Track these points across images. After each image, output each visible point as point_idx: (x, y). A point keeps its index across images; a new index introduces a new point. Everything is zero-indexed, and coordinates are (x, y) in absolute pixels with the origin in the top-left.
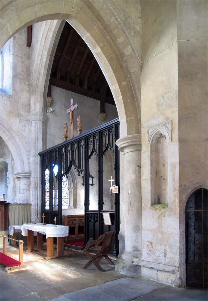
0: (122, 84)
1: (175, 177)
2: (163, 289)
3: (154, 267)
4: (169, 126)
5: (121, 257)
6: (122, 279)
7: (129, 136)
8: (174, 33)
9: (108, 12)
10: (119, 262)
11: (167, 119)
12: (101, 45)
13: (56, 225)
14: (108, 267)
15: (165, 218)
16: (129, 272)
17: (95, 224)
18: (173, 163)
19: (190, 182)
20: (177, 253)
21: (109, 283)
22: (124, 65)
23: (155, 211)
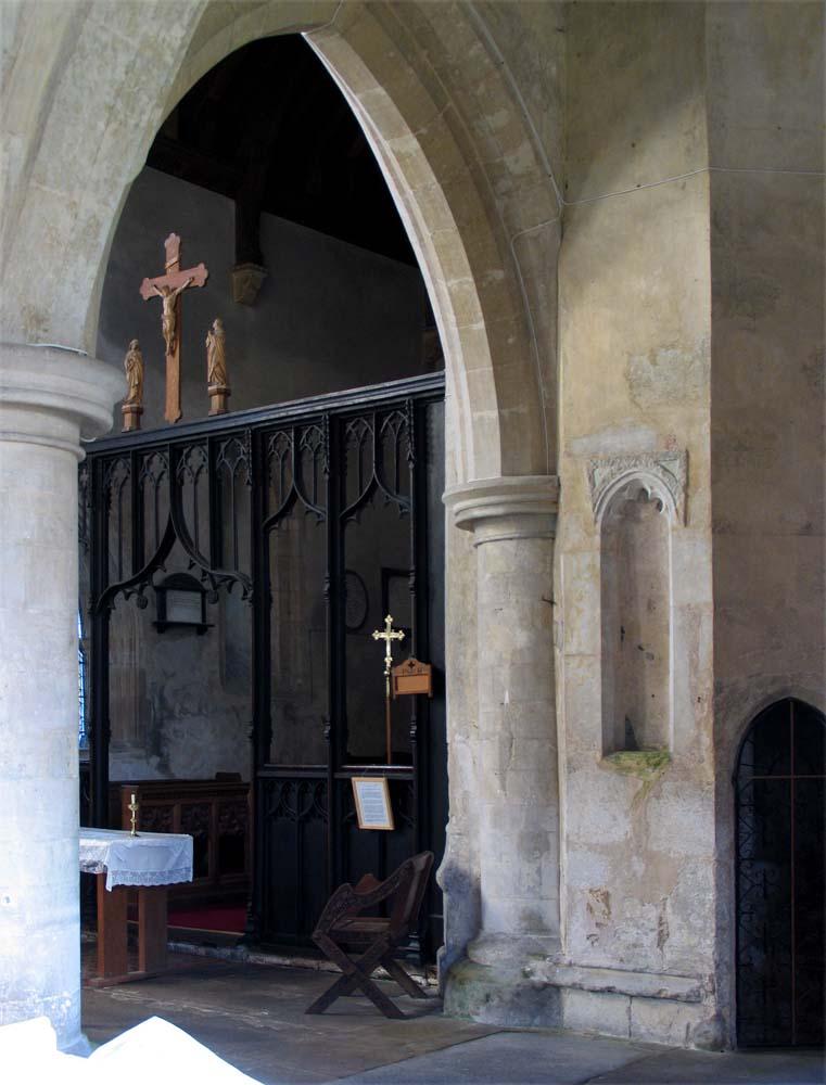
1: (697, 656)
4: (676, 468)
8: (697, 133)
9: (461, 24)
12: (424, 131)
13: (138, 833)
15: (661, 801)
16: (512, 1014)
18: (689, 605)
19: (750, 677)
23: (622, 775)
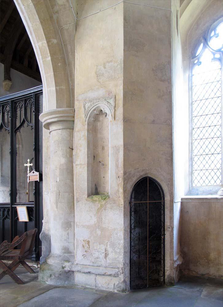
0: (51, 41)
1: (118, 163)
2: (106, 297)
3: (92, 271)
4: (112, 101)
5: (46, 261)
6: (51, 291)
7: (60, 109)
10: (44, 269)
11: (109, 94)
14: (28, 276)
17: (5, 220)
18: (115, 146)
20: (120, 252)
21: (35, 299)
22: (55, 17)
